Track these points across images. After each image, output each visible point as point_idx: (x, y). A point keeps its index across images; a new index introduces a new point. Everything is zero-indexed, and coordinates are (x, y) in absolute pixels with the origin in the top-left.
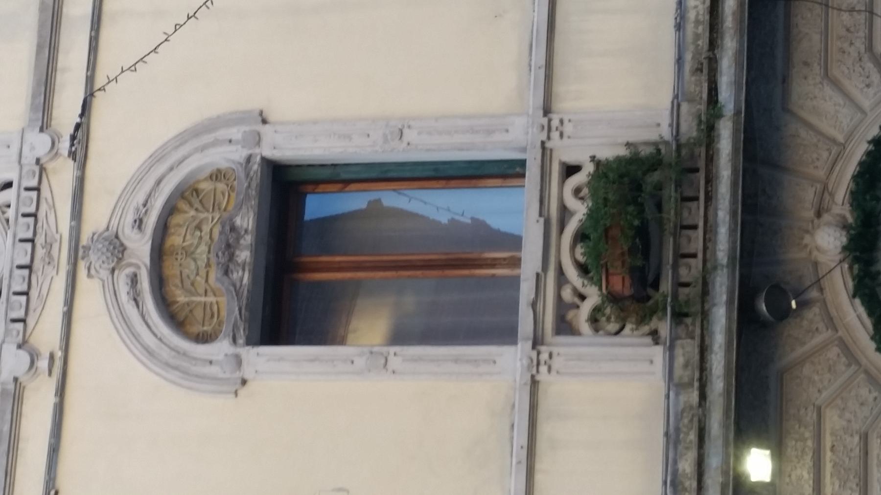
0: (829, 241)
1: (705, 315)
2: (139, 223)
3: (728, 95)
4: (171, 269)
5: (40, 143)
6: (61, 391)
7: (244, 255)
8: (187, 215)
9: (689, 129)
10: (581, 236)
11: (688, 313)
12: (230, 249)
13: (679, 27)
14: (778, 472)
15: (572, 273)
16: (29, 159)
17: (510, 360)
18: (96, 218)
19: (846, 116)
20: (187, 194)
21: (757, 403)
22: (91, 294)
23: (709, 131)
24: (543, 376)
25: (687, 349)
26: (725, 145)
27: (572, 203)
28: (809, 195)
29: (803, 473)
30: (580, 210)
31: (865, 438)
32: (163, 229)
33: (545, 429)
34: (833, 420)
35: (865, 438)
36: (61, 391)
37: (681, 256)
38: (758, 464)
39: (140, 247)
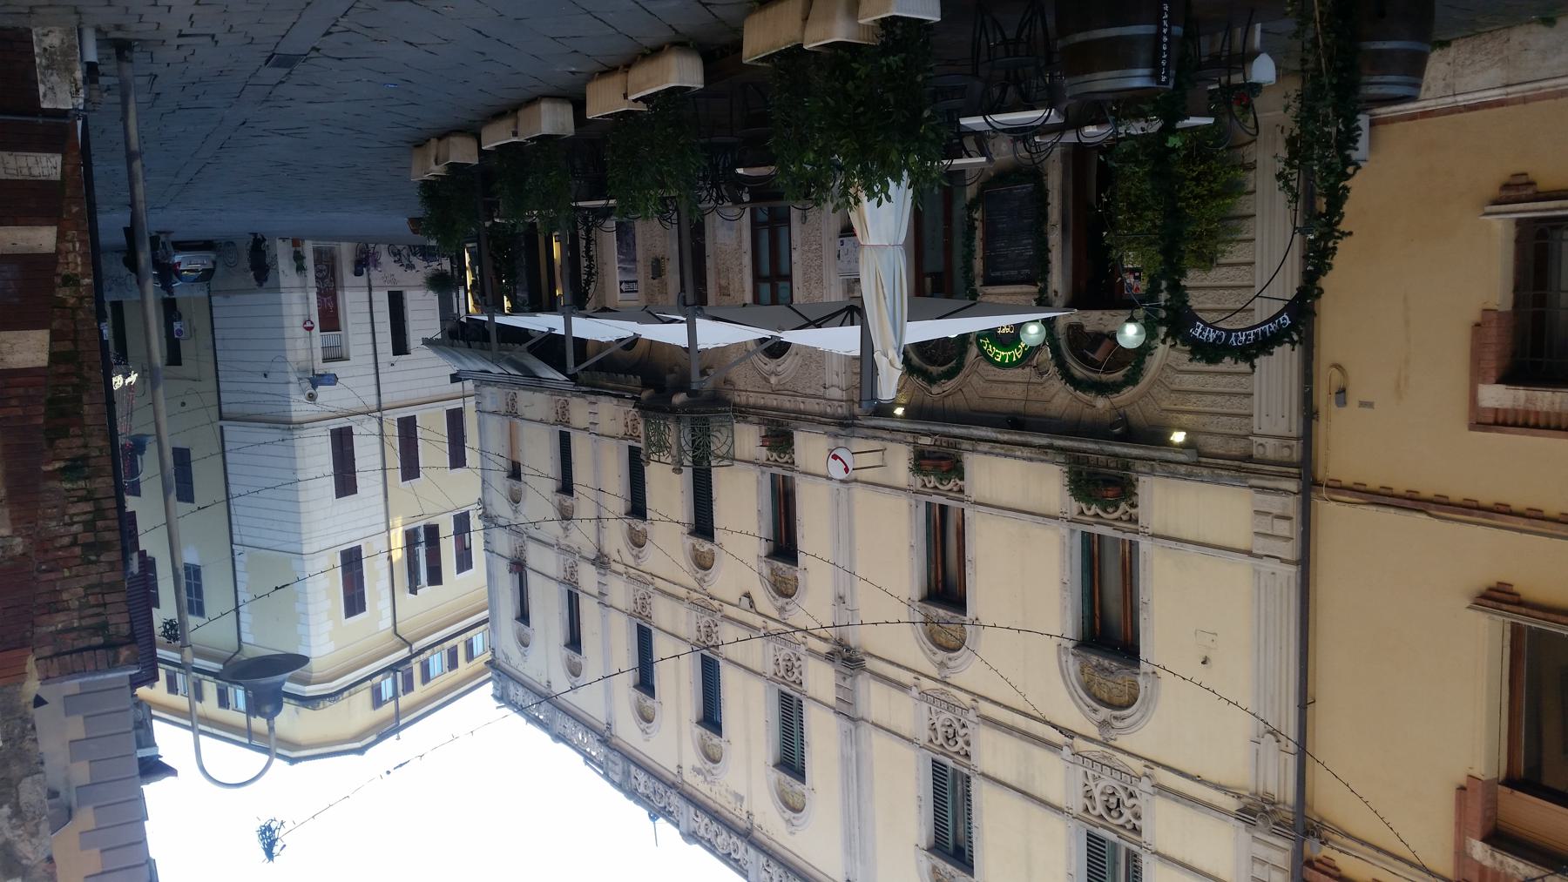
0: (1101, 403)
1: (1125, 456)
2: (1095, 711)
3: (1044, 441)
4: (1116, 701)
5: (1066, 751)
6: (986, 699)
7: (1106, 663)
8: (942, 639)
9: (1061, 459)
10: (1105, 511)
11: (1126, 463)
12: (1104, 669)
13: (1031, 460)
14: (1180, 429)
15: (1116, 515)
16: (1071, 758)
17: (1145, 545)
18: (1093, 731)
19: (1062, 394)
20: (1088, 689)
21: (1155, 436)
22: (1122, 742)
23: (1062, 450)
24: (1150, 531)
25: (1138, 465)
26: (1075, 444)
27: (1092, 512)
28: (1088, 411)
29: (1185, 418)
30: (1095, 509)
31: (1173, 391)
32: (1101, 702)
33: (1171, 533)
34: (1165, 405)
35: (1173, 391)
36: (986, 699)
37: (1107, 466)
38: (1178, 437)
39: (1105, 713)
